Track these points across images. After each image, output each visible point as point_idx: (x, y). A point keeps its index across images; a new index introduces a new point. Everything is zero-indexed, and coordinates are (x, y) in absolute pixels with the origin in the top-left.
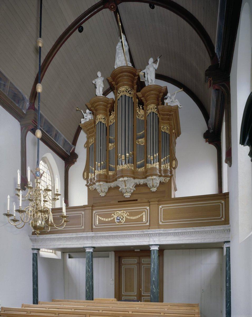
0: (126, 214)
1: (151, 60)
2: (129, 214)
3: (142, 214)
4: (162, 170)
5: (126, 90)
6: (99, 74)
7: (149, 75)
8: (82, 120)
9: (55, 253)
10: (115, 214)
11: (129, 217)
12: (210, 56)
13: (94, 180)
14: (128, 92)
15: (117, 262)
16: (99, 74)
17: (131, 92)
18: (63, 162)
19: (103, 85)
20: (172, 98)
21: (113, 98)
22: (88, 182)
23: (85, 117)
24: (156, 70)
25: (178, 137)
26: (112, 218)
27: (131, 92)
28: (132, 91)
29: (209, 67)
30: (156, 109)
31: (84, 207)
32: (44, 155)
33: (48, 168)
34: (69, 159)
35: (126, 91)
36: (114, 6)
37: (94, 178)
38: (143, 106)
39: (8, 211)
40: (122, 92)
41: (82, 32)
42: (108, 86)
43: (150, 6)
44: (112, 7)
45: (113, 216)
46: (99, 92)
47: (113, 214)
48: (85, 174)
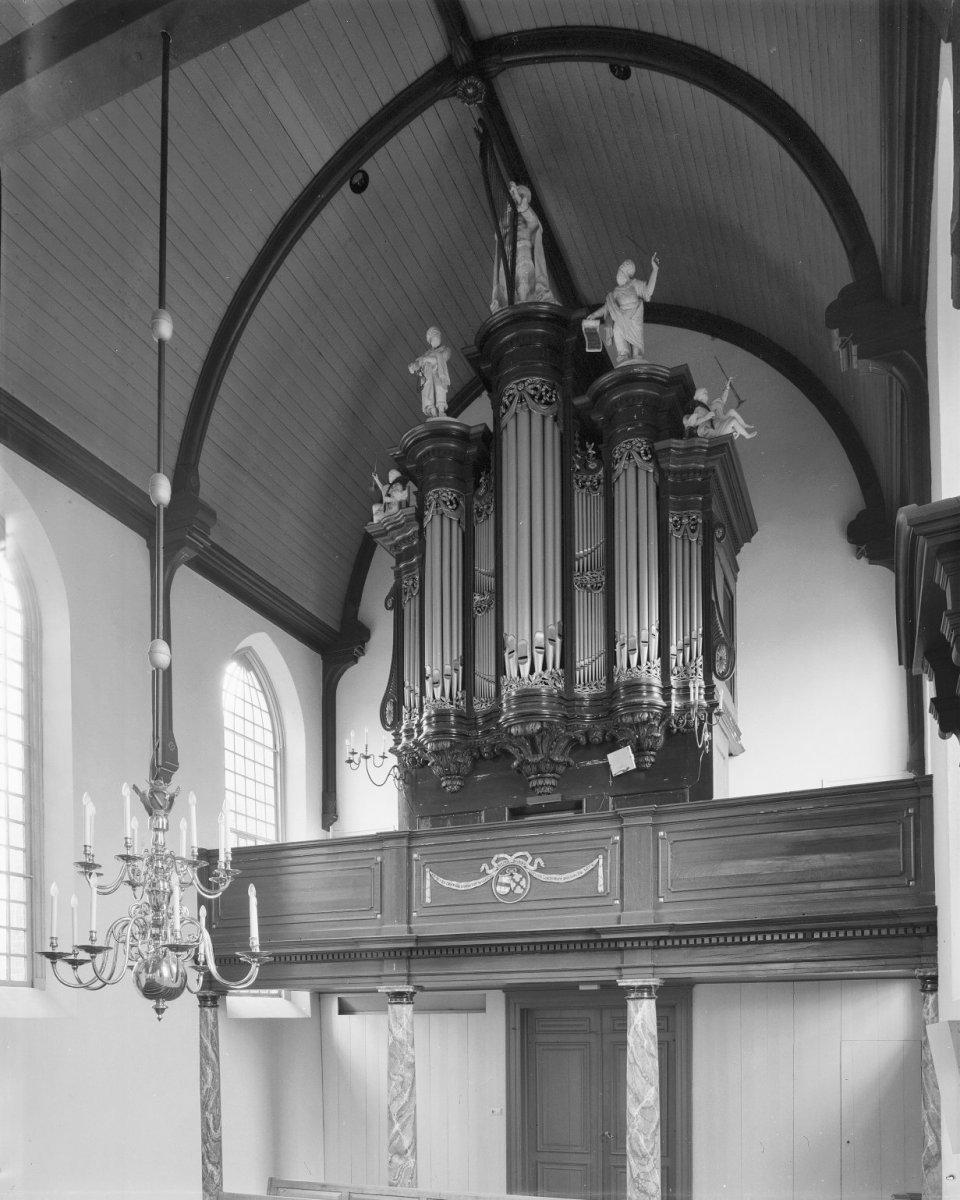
0: (532, 864)
1: (627, 269)
2: (542, 864)
3: (595, 862)
4: (671, 687)
5: (532, 392)
6: (433, 337)
7: (623, 330)
8: (375, 508)
9: (288, 998)
10: (493, 862)
11: (543, 877)
12: (846, 248)
13: (420, 732)
14: (541, 398)
15: (515, 1029)
16: (433, 337)
17: (551, 397)
18: (317, 659)
19: (445, 377)
20: (713, 408)
21: (485, 425)
22: (397, 742)
23: (386, 499)
24: (645, 304)
25: (746, 544)
26: (482, 881)
27: (551, 397)
28: (554, 392)
29: (842, 291)
30: (646, 455)
31: (381, 838)
32: (238, 644)
33: (260, 683)
34: (334, 645)
35: (533, 397)
36: (475, 87)
37: (419, 725)
38: (600, 446)
39: (126, 838)
40: (517, 398)
41: (364, 194)
42: (467, 373)
43: (612, 69)
44: (470, 91)
45: (485, 873)
46: (435, 397)
47: (484, 866)
48: (389, 707)
